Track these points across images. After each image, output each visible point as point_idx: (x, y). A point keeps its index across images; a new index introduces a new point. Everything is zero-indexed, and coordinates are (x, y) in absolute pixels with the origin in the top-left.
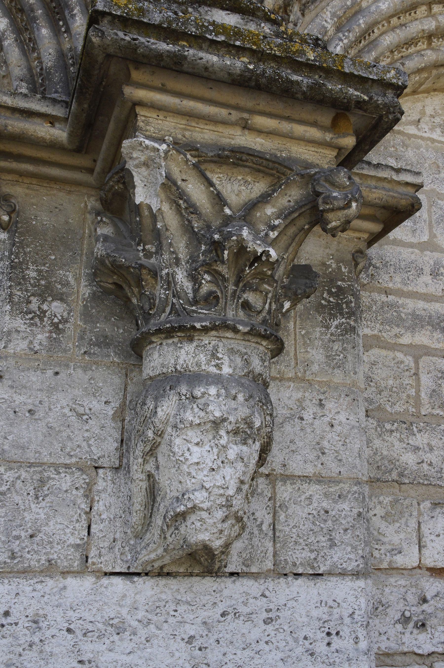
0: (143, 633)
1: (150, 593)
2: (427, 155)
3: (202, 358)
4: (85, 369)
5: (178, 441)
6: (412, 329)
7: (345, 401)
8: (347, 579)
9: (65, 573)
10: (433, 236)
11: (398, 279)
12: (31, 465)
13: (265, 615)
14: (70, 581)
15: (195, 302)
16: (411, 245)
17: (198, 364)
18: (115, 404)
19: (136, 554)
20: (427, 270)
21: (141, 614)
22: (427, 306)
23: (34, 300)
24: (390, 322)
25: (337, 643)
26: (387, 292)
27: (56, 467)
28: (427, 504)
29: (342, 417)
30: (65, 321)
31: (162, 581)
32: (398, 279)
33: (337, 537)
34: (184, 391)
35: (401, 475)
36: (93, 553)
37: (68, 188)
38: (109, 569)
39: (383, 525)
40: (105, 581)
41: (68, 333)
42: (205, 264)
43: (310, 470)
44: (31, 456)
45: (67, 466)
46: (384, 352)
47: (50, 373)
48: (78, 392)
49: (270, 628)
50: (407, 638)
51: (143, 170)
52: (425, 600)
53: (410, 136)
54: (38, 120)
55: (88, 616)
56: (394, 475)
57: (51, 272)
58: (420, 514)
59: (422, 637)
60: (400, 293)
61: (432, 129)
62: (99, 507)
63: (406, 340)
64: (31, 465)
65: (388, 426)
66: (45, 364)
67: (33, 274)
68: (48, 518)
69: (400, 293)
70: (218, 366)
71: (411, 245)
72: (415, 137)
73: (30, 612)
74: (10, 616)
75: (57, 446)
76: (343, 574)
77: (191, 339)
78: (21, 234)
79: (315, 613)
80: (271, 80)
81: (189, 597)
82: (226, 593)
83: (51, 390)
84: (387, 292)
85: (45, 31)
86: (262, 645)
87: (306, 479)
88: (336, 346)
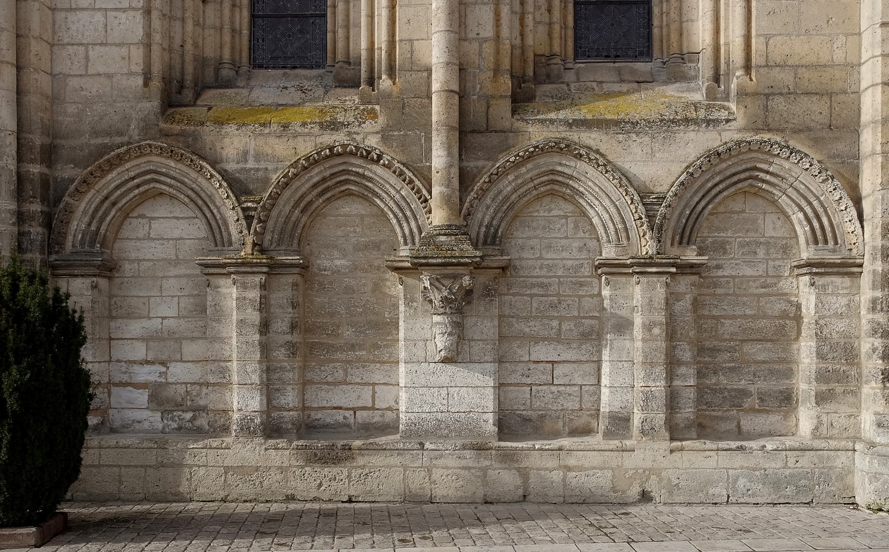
2: (541, 223)
6: (531, 288)
7: (489, 320)
10: (541, 254)
11: (526, 272)
16: (532, 259)
20: (538, 267)
22: (536, 280)
24: (523, 287)
26: (523, 277)
28: (533, 343)
29: (488, 324)
30: (417, 307)
32: (526, 272)
33: (486, 354)
35: (524, 334)
39: (517, 349)
43: (479, 338)
46: (520, 297)
50: (523, 380)
52: (529, 370)
53: (535, 217)
56: (522, 335)
57: (413, 296)
58: (530, 346)
59: (528, 379)
60: (527, 277)
61: (544, 212)
63: (528, 292)
65: (520, 320)
69: (527, 277)
71: (532, 259)
72: (537, 216)
74: (70, 296)
76: (488, 362)
84: (523, 277)
87: (477, 340)
88: (488, 306)
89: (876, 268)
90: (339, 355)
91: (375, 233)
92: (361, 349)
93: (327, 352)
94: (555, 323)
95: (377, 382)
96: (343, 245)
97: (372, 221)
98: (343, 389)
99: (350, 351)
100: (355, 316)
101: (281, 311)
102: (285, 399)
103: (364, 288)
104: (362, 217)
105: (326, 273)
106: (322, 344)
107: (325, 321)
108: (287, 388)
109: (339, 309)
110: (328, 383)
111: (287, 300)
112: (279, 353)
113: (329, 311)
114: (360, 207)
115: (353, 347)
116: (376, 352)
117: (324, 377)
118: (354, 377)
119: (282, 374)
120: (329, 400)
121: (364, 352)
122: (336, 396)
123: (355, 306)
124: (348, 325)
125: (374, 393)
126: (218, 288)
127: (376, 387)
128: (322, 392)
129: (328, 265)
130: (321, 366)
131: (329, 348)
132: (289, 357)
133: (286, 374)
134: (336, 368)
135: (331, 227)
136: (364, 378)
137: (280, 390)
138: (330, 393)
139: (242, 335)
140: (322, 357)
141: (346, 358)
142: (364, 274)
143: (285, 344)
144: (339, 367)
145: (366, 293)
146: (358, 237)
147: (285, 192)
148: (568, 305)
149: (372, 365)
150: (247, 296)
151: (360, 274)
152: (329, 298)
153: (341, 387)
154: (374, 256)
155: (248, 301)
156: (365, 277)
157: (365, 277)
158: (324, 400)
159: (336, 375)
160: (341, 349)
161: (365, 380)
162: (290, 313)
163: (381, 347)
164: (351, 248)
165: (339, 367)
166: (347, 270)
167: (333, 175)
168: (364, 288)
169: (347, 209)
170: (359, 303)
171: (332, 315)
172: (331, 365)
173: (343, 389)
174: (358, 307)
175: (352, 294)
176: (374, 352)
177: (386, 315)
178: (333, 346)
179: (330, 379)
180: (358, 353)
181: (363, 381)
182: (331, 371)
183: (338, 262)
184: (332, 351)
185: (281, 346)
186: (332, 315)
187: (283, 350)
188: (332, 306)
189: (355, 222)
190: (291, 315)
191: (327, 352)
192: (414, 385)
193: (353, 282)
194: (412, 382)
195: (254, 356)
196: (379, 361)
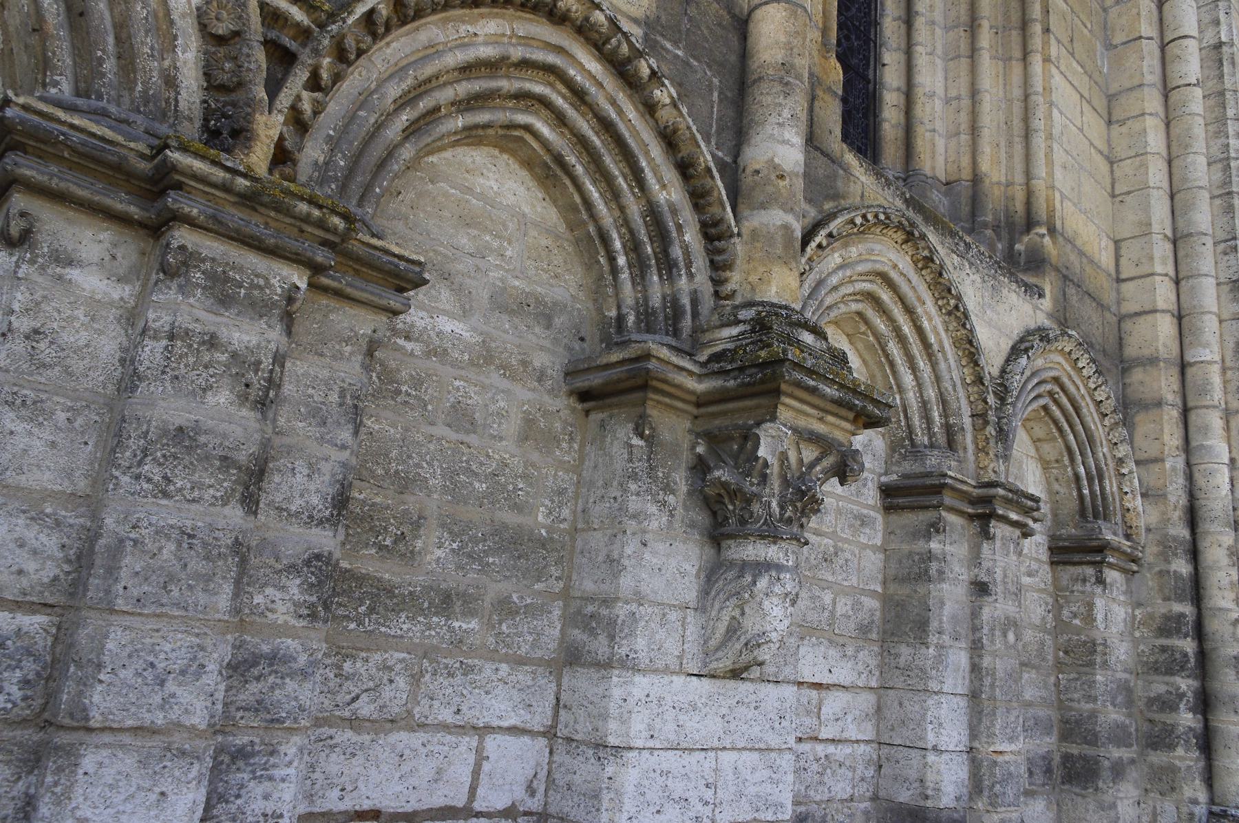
0: (704, 711)
1: (707, 687)
3: (781, 555)
4: (684, 543)
5: (766, 603)
8: (1215, 686)
9: (673, 673)
12: (659, 604)
13: (754, 704)
14: (674, 678)
15: (781, 520)
17: (779, 559)
18: (696, 567)
19: (705, 665)
21: (703, 700)
23: (661, 492)
25: (784, 723)
27: (670, 606)
31: (713, 681)
34: (774, 574)
36: (685, 661)
37: (678, 413)
38: (691, 672)
40: (688, 679)
41: (677, 517)
42: (791, 500)
44: (659, 599)
45: (674, 606)
47: (668, 544)
48: (680, 558)
49: (756, 712)
51: (769, 439)
54: (684, 373)
55: (681, 699)
62: (688, 633)
64: (659, 604)
66: (666, 538)
67: (661, 475)
68: (666, 639)
70: (787, 561)
73: (658, 695)
75: (671, 592)
77: (775, 543)
78: (656, 446)
79: (776, 705)
80: (848, 403)
81: (722, 691)
82: (740, 690)
83: (668, 556)
85: (655, 278)
86: (753, 722)
89: (1179, 570)
90: (403, 625)
91: (545, 276)
92: (469, 613)
93: (372, 610)
94: (827, 598)
95: (495, 723)
96: (468, 281)
97: (544, 242)
98: (400, 746)
99: (436, 614)
100: (466, 503)
101: (315, 431)
102: (266, 797)
103: (500, 424)
104: (523, 221)
105: (409, 346)
106: (361, 579)
107: (378, 500)
108: (283, 749)
109: (425, 472)
110: (354, 723)
111: (342, 395)
112: (279, 595)
113: (397, 472)
114: (521, 191)
115: (446, 602)
116: (504, 627)
117: (348, 697)
118: (436, 704)
119: (272, 688)
120: (349, 788)
121: (474, 624)
122: (373, 771)
123: (469, 471)
124: (443, 525)
125: (481, 758)
126: (70, 263)
127: (492, 744)
128: (334, 756)
129: (420, 324)
130: (346, 657)
131: (377, 595)
132: (313, 616)
133: (290, 685)
134: (390, 669)
135: (446, 214)
136: (464, 708)
137: (253, 754)
138: (359, 759)
139: (166, 495)
140: (352, 626)
141: (423, 637)
142: (505, 384)
143: (308, 563)
144: (399, 666)
145: (501, 439)
146: (507, 271)
147: (397, 39)
148: (847, 561)
149: (488, 668)
150: (224, 334)
151: (495, 378)
152: (407, 430)
153: (394, 737)
154: (534, 339)
155: (223, 358)
156: (506, 392)
157: (506, 392)
158: (332, 786)
159: (387, 692)
160: (409, 603)
161: (468, 716)
162: (344, 447)
163: (517, 613)
164: (485, 295)
165: (399, 666)
166: (466, 357)
167: (525, 64)
168: (500, 424)
169: (492, 183)
170: (482, 464)
171: (405, 484)
172: (377, 657)
173: (400, 746)
174: (476, 474)
175: (468, 432)
176: (500, 624)
177: (540, 518)
178: (390, 592)
179: (365, 708)
180: (456, 624)
181: (458, 720)
182: (371, 678)
183: (447, 325)
184: (386, 609)
185: (292, 569)
186: (405, 484)
187: (294, 587)
188: (410, 457)
189: (506, 228)
190: (345, 455)
191: (372, 610)
192: (650, 744)
193: (476, 399)
194: (647, 734)
195: (203, 598)
196: (506, 654)
